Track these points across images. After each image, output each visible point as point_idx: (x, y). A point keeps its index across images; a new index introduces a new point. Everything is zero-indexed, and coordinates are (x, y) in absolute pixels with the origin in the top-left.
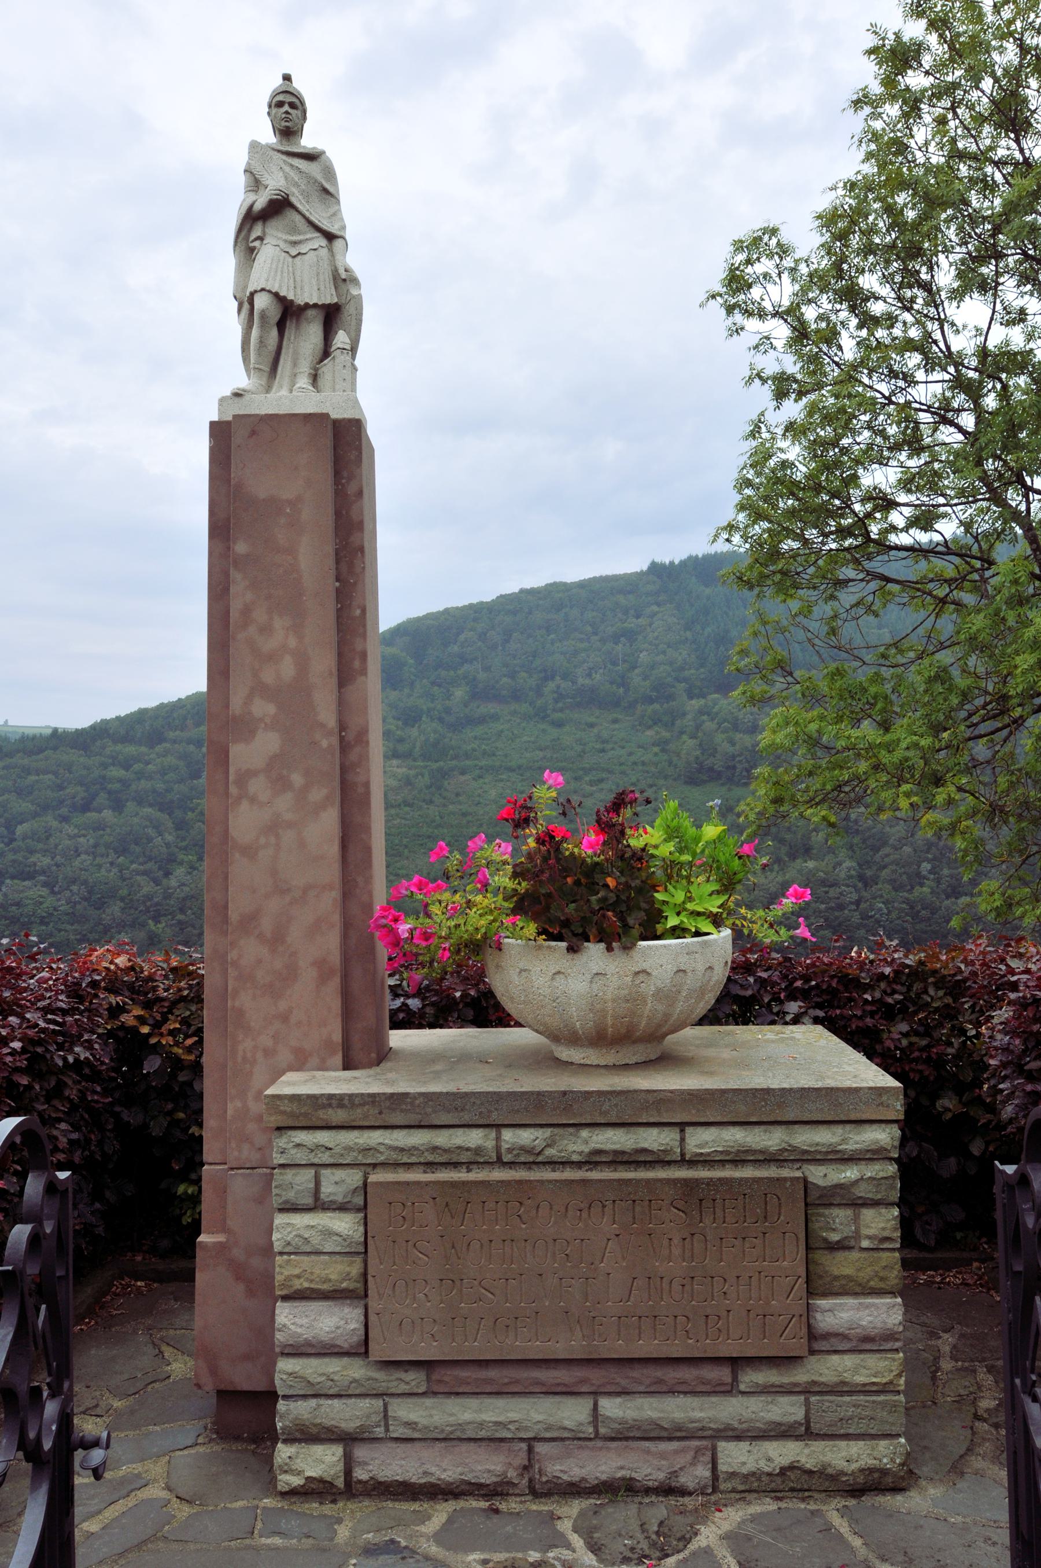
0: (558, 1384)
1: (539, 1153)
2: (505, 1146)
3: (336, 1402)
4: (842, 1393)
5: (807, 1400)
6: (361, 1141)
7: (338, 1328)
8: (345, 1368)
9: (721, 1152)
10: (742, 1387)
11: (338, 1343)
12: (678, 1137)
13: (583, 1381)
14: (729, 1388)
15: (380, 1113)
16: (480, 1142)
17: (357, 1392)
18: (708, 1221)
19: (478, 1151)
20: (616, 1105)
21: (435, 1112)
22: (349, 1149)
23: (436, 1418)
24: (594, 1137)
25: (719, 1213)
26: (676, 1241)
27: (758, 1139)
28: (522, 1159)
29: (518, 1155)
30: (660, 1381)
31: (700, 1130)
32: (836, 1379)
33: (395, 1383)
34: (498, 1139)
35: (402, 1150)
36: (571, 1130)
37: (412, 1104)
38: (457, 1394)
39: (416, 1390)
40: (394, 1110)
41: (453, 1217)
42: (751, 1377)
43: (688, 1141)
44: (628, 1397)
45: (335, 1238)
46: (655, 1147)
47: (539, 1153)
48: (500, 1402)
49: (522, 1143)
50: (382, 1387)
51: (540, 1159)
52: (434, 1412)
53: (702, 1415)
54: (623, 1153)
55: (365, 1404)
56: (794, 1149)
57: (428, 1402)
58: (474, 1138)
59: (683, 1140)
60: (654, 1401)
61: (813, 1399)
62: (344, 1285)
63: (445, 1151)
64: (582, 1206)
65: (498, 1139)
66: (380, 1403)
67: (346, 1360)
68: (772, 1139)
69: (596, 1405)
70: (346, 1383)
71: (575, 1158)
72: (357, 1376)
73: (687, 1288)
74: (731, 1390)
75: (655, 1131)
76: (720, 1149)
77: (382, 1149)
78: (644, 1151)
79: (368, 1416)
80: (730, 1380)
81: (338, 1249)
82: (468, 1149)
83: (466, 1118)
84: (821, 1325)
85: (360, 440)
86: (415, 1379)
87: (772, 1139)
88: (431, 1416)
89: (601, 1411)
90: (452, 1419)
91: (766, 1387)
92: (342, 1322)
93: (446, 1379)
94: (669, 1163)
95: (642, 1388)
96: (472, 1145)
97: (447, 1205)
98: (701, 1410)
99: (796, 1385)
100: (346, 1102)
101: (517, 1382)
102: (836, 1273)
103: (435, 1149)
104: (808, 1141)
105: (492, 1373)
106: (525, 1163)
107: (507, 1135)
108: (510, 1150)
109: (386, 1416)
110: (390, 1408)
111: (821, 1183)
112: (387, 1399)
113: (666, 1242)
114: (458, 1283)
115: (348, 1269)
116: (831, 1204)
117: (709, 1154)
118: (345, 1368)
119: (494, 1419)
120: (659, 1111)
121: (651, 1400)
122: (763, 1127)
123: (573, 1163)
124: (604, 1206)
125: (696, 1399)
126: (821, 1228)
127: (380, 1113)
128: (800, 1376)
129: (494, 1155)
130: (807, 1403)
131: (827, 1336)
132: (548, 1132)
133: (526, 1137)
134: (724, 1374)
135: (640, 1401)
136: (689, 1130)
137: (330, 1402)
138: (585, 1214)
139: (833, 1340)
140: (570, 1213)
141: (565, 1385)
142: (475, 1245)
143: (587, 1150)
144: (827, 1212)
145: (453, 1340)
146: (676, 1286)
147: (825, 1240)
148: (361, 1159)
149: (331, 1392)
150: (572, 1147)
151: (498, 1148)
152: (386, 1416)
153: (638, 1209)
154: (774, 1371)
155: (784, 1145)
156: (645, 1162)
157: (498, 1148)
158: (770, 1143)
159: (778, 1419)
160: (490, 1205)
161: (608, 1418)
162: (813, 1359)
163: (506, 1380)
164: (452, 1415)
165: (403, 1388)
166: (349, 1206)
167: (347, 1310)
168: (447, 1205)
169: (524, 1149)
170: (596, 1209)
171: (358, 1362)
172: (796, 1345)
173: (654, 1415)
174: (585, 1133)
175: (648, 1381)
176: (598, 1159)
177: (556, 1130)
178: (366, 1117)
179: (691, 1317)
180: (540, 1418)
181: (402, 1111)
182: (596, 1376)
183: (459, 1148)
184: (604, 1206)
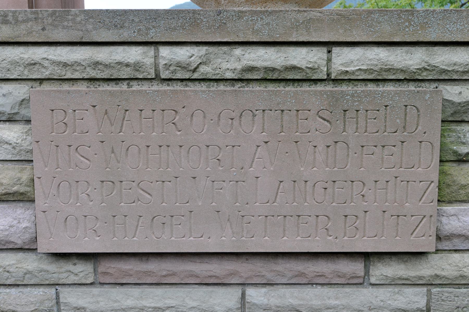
0: (211, 277)
1: (194, 70)
2: (162, 62)
3: (13, 291)
4: (459, 286)
5: (429, 291)
6: (26, 56)
7: (11, 226)
8: (19, 262)
9: (365, 71)
10: (373, 280)
11: (12, 239)
12: (325, 56)
13: (232, 274)
14: (361, 281)
15: (43, 29)
16: (139, 58)
17: (32, 282)
18: (351, 129)
19: (137, 66)
20: (268, 24)
21: (95, 29)
22: (15, 63)
23: (102, 304)
24: (247, 56)
25: (362, 123)
26: (321, 148)
27: (399, 59)
28: (179, 76)
29: (174, 72)
30: (301, 274)
31: (346, 50)
32: (456, 274)
33: (65, 275)
34: (156, 57)
35: (65, 65)
36: (225, 48)
37: (73, 20)
38: (122, 284)
39: (84, 281)
40: (56, 26)
41: (112, 125)
42: (381, 271)
43: (334, 60)
44: (272, 288)
45: (6, 146)
46: (303, 64)
47: (194, 70)
48: (159, 291)
49: (178, 59)
50: (54, 278)
51: (196, 76)
52: (100, 299)
53: (337, 302)
54: (273, 70)
55: (40, 291)
56: (433, 68)
57: (96, 290)
58: (133, 54)
59: (329, 60)
60: (295, 291)
61: (435, 290)
62: (15, 188)
63: (106, 66)
64: (233, 115)
65: (156, 57)
66: (53, 291)
67: (20, 255)
68: (413, 59)
69: (243, 294)
70: (21, 274)
71: (229, 75)
72: (30, 268)
73: (329, 190)
74: (362, 282)
75: (303, 50)
76: (364, 67)
77: (46, 63)
78: (294, 68)
79: (42, 302)
80: (362, 274)
81: (9, 157)
82: (127, 65)
83: (126, 36)
84: (447, 227)
85: (183, 11)
86: (83, 270)
87: (413, 59)
88: (98, 302)
89: (248, 299)
90: (116, 305)
91: (394, 279)
92: (15, 222)
93: (109, 271)
94: (316, 81)
95: (284, 281)
96: (131, 60)
97: (106, 113)
98: (337, 299)
99: (420, 278)
100: (10, 18)
101: (174, 274)
102: (463, 182)
103: (97, 64)
104: (447, 62)
105: (152, 266)
106: (182, 80)
107: (165, 51)
108: (167, 66)
109: (58, 303)
110: (61, 296)
111: (456, 99)
112: (59, 288)
113: (311, 149)
114: (118, 184)
115: (19, 175)
116: (462, 121)
117: (353, 73)
118: (19, 262)
119: (153, 305)
120: (308, 30)
121: (292, 290)
122: (405, 49)
123: (227, 80)
124: (254, 116)
125: (332, 290)
126: (452, 143)
127: (43, 29)
128: (424, 270)
129: (152, 72)
130: (429, 293)
131: (449, 237)
132: (203, 50)
133: (182, 54)
134: (357, 267)
135: (283, 290)
136: (336, 50)
137: (8, 290)
138: (236, 122)
139: (456, 241)
140: (222, 121)
141: (217, 277)
142: (134, 149)
143: (239, 67)
144: (459, 128)
145: (114, 236)
146: (319, 189)
147: (455, 152)
148: (27, 74)
149: (8, 282)
150: (225, 66)
151: (156, 65)
152: (58, 303)
153: (286, 117)
154: (402, 266)
155: (424, 65)
156: (294, 81)
157: (156, 65)
158: (411, 62)
159: (403, 306)
160: (147, 113)
161: (254, 304)
162: (437, 256)
163: (164, 273)
164: (116, 301)
165: (73, 279)
166: (17, 118)
167: (19, 211)
168: (106, 113)
169: (181, 66)
170: (247, 117)
171: (31, 256)
172: (426, 243)
173: (295, 302)
174: (238, 51)
175: (290, 274)
176: (249, 76)
177: (212, 49)
178: (30, 33)
179: (331, 217)
180: (195, 304)
181: (64, 27)
182: (244, 268)
183: (119, 63)
184: (254, 116)
